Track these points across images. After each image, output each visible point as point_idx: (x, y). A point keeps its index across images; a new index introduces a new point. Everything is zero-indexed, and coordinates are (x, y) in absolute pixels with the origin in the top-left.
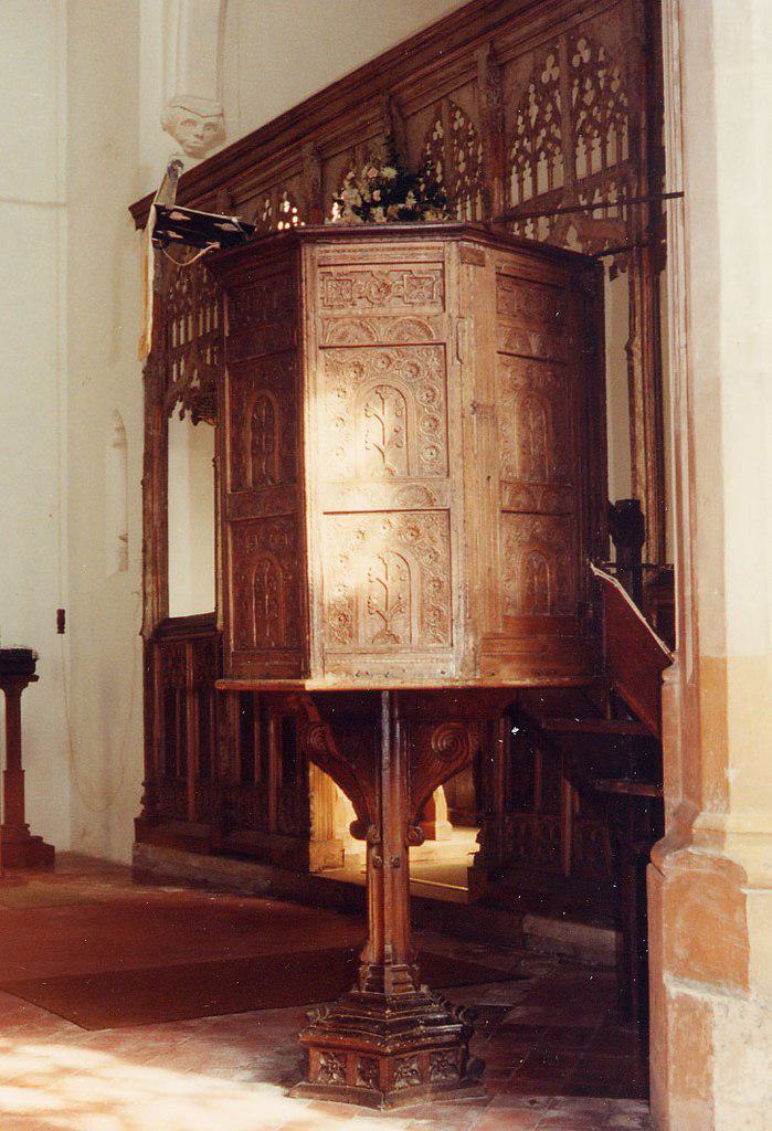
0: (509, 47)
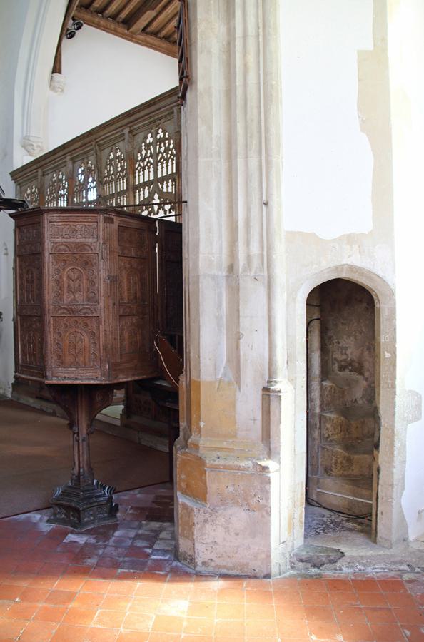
0: (136, 129)
